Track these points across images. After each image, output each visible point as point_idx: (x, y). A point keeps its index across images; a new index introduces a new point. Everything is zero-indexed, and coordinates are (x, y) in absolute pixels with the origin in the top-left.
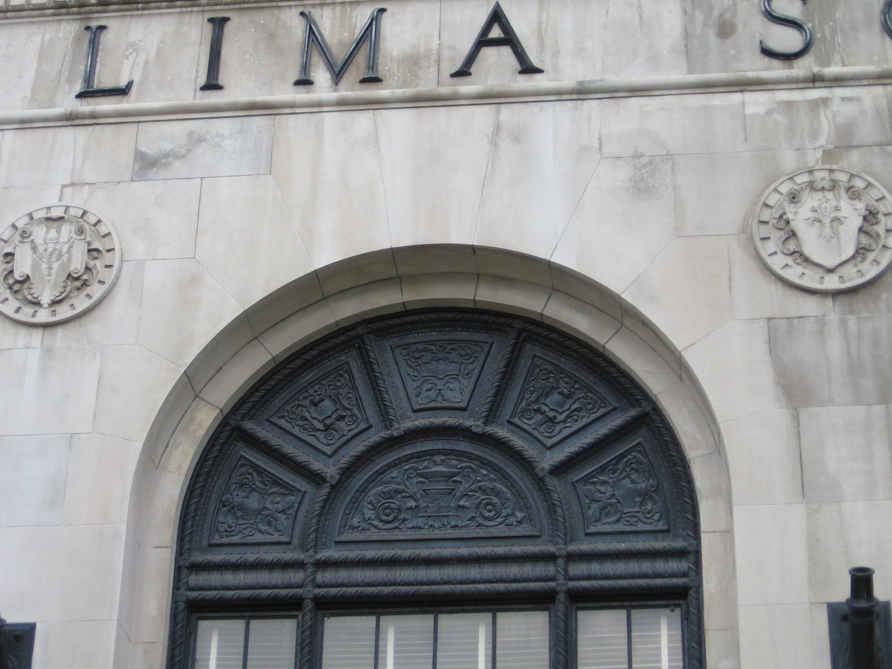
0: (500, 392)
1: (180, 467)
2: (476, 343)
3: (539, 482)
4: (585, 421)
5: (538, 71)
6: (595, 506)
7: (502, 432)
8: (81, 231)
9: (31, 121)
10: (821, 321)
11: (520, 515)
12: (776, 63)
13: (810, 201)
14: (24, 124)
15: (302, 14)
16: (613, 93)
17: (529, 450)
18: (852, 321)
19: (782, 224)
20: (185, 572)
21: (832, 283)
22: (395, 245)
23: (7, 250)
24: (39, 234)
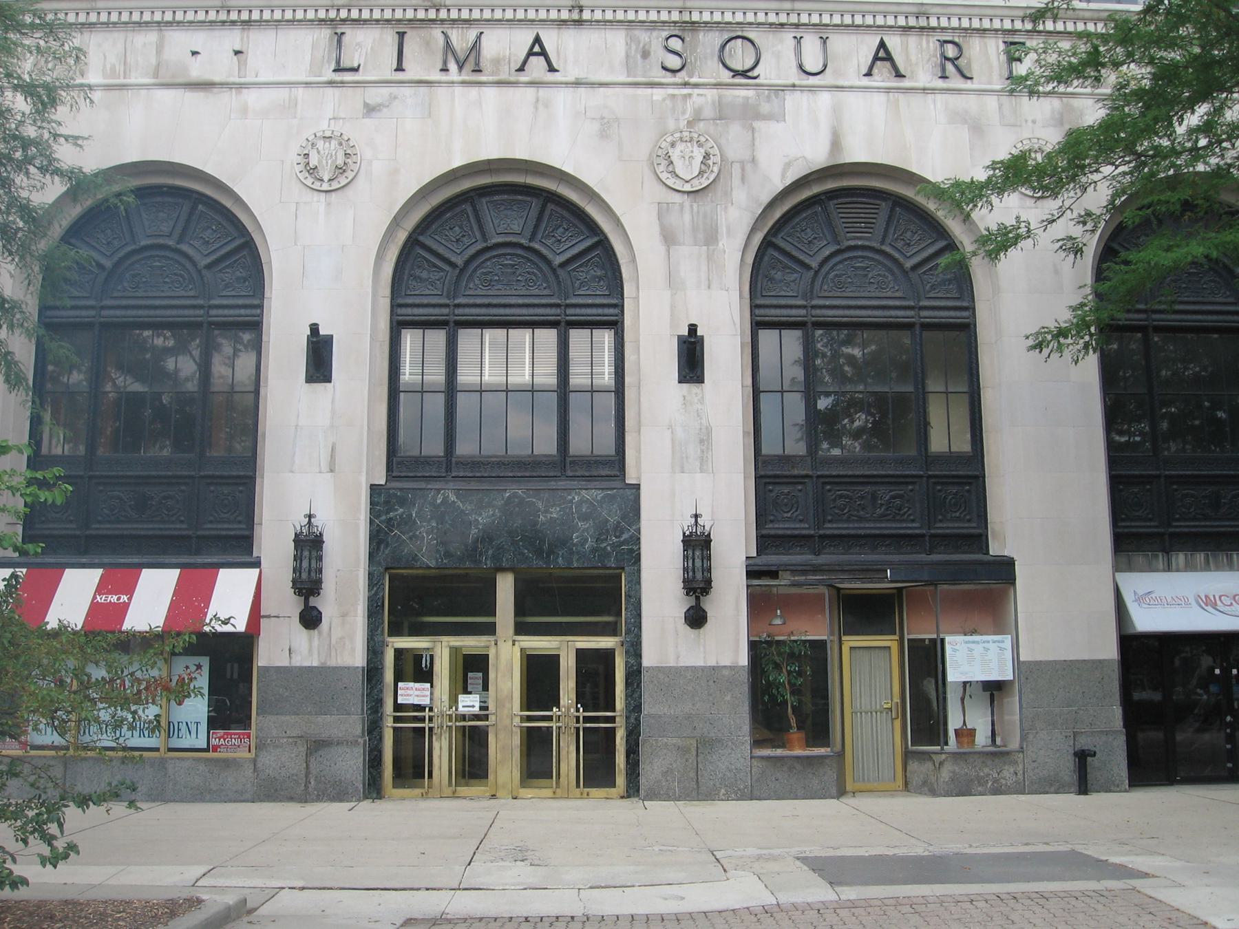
0: (536, 227)
1: (391, 260)
2: (525, 202)
3: (554, 271)
4: (574, 242)
5: (557, 71)
6: (578, 282)
7: (537, 246)
8: (341, 144)
9: (311, 83)
10: (682, 206)
11: (545, 285)
12: (668, 74)
13: (680, 147)
14: (308, 84)
15: (443, 32)
16: (592, 85)
17: (550, 256)
18: (695, 206)
19: (667, 158)
20: (395, 308)
21: (687, 188)
22: (490, 158)
23: (305, 152)
24: (320, 144)
